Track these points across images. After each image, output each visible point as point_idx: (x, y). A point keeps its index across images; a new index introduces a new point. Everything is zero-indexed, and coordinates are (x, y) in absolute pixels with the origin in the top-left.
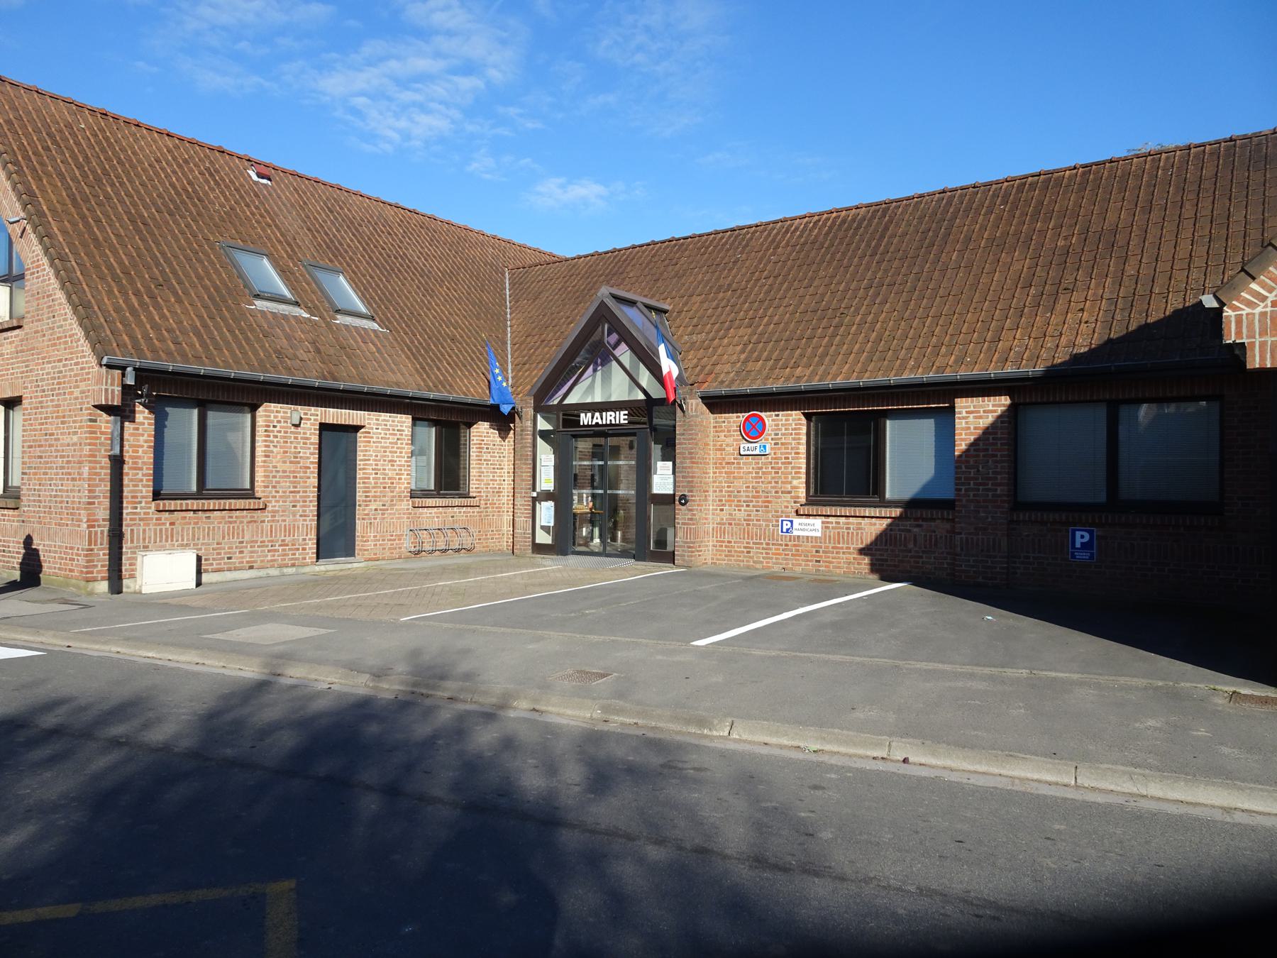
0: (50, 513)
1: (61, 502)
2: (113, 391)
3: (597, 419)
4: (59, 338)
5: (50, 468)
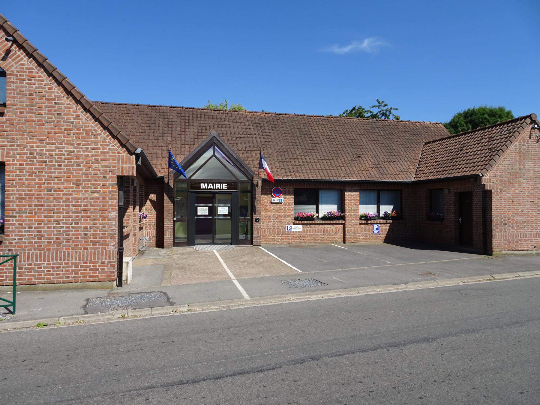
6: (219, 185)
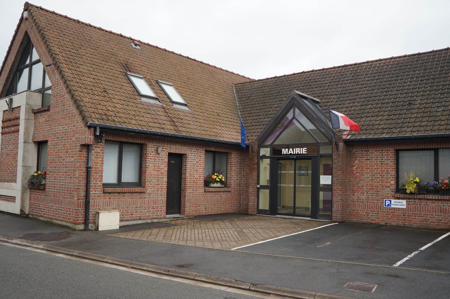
0: (60, 192)
1: (65, 188)
2: (90, 137)
3: (291, 151)
4: (66, 115)
5: (60, 172)
6: (299, 149)
